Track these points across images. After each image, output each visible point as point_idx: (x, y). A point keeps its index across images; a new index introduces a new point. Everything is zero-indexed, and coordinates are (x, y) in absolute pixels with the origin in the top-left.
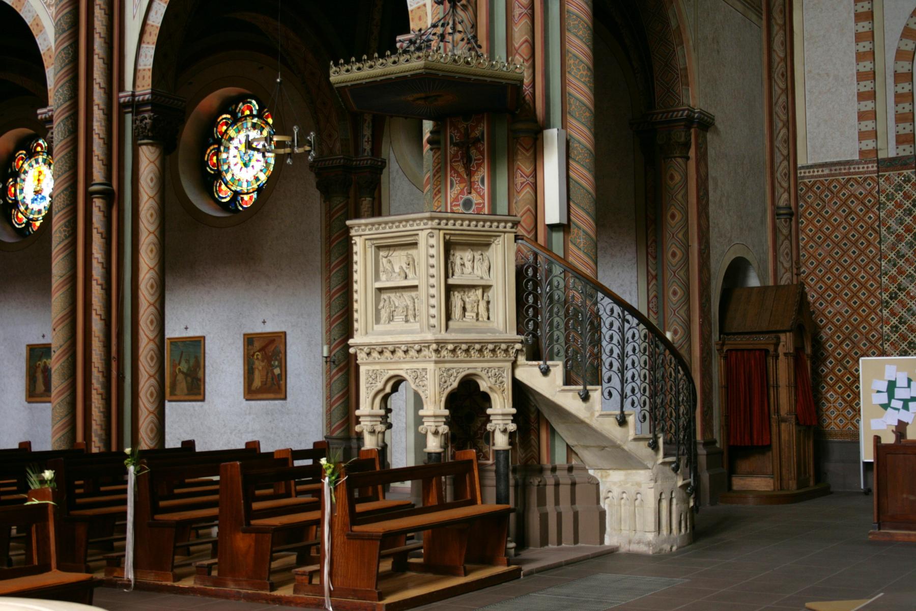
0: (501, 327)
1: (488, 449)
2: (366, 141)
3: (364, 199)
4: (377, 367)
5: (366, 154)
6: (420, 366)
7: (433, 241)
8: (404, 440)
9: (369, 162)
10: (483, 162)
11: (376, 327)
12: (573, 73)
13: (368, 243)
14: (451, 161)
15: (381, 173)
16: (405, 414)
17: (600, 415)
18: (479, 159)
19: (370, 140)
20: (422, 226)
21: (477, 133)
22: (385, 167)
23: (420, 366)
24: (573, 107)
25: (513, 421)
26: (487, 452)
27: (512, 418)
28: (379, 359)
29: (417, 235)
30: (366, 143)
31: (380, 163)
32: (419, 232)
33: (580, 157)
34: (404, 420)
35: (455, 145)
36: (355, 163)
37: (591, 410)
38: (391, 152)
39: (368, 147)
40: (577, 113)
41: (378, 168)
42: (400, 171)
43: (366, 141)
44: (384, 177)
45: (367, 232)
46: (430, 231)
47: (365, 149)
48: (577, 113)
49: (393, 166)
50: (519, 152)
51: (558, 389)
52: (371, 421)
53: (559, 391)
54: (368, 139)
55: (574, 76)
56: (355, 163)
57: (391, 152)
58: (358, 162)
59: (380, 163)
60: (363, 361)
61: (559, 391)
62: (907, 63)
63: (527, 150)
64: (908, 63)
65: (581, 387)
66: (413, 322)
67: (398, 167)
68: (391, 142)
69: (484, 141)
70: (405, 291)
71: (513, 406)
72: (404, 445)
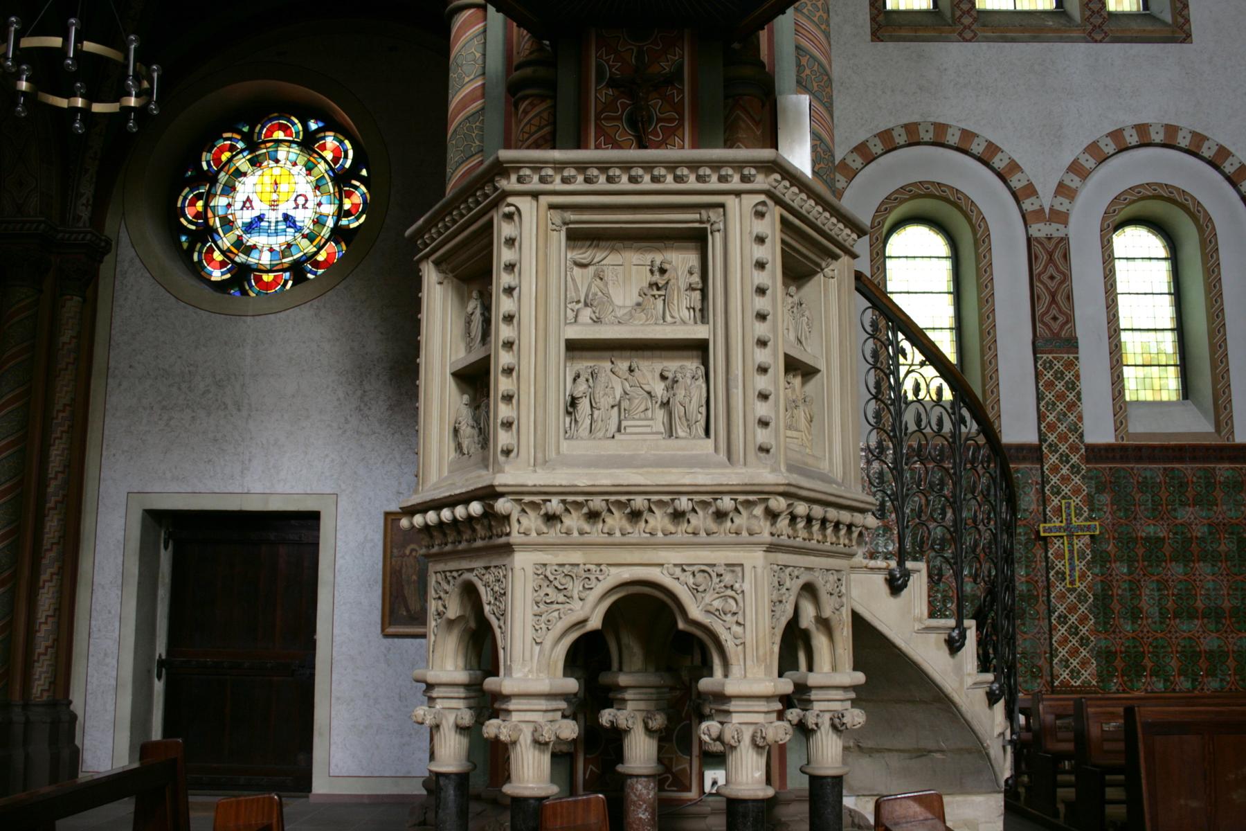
0: (838, 474)
1: (687, 766)
2: (83, 205)
3: (68, 297)
4: (576, 557)
5: (81, 225)
6: (720, 557)
7: (761, 227)
8: (111, 707)
9: (89, 236)
10: (681, 125)
11: (565, 446)
12: (805, 11)
13: (556, 216)
14: (597, 118)
15: (101, 262)
16: (115, 662)
17: (975, 684)
18: (671, 120)
19: (91, 202)
20: (735, 183)
21: (665, 66)
22: (108, 251)
23: (720, 557)
24: (808, 71)
25: (855, 703)
26: (684, 770)
27: (853, 695)
28: (581, 533)
29: (722, 206)
30: (84, 208)
31: (103, 244)
32: (731, 201)
33: (822, 165)
34: (114, 673)
35: (613, 83)
36: (60, 235)
37: (958, 670)
38: (123, 229)
39: (85, 213)
40: (815, 84)
41: (100, 249)
42: (137, 260)
43: (83, 205)
44: (105, 269)
45: (557, 185)
46: (762, 198)
47: (80, 217)
48: (815, 84)
49: (126, 251)
50: (742, 124)
51: (917, 626)
52: (546, 711)
53: (918, 632)
54: (88, 201)
55: (808, 17)
56: (60, 235)
57: (123, 229)
58: (67, 236)
59: (103, 244)
60: (523, 539)
61: (918, 632)
62: (1114, 146)
63: (757, 123)
64: (1162, 138)
65: (952, 622)
66: (685, 438)
67: (134, 254)
68: (123, 214)
69: (681, 81)
70: (643, 358)
71: (856, 668)
72: (109, 717)
